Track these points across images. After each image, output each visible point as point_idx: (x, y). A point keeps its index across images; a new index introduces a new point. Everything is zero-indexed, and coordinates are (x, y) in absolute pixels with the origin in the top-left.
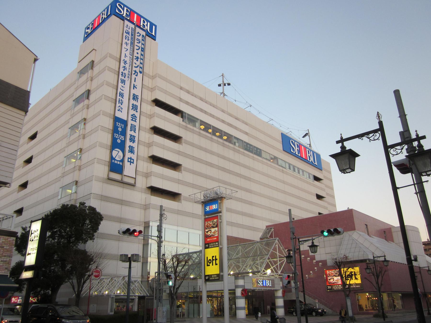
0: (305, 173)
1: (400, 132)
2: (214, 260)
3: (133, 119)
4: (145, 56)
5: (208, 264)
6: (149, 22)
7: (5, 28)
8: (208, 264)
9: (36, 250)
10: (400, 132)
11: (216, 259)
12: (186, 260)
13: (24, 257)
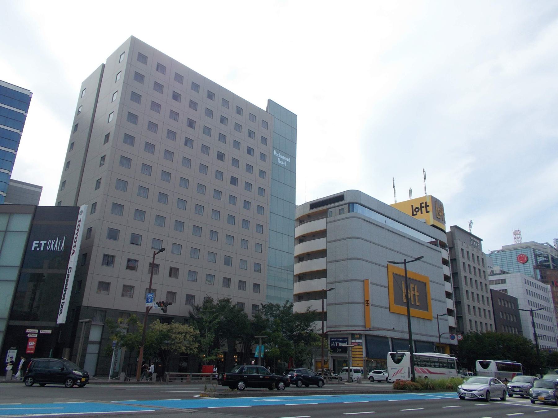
0: (256, 183)
1: (41, 188)
2: (423, 207)
3: (370, 329)
4: (57, 388)
5: (414, 213)
6: (73, 386)
7: (57, 388)
8: (414, 213)
9: (70, 268)
10: (41, 188)
11: (427, 206)
12: (200, 334)
13: (108, 292)
